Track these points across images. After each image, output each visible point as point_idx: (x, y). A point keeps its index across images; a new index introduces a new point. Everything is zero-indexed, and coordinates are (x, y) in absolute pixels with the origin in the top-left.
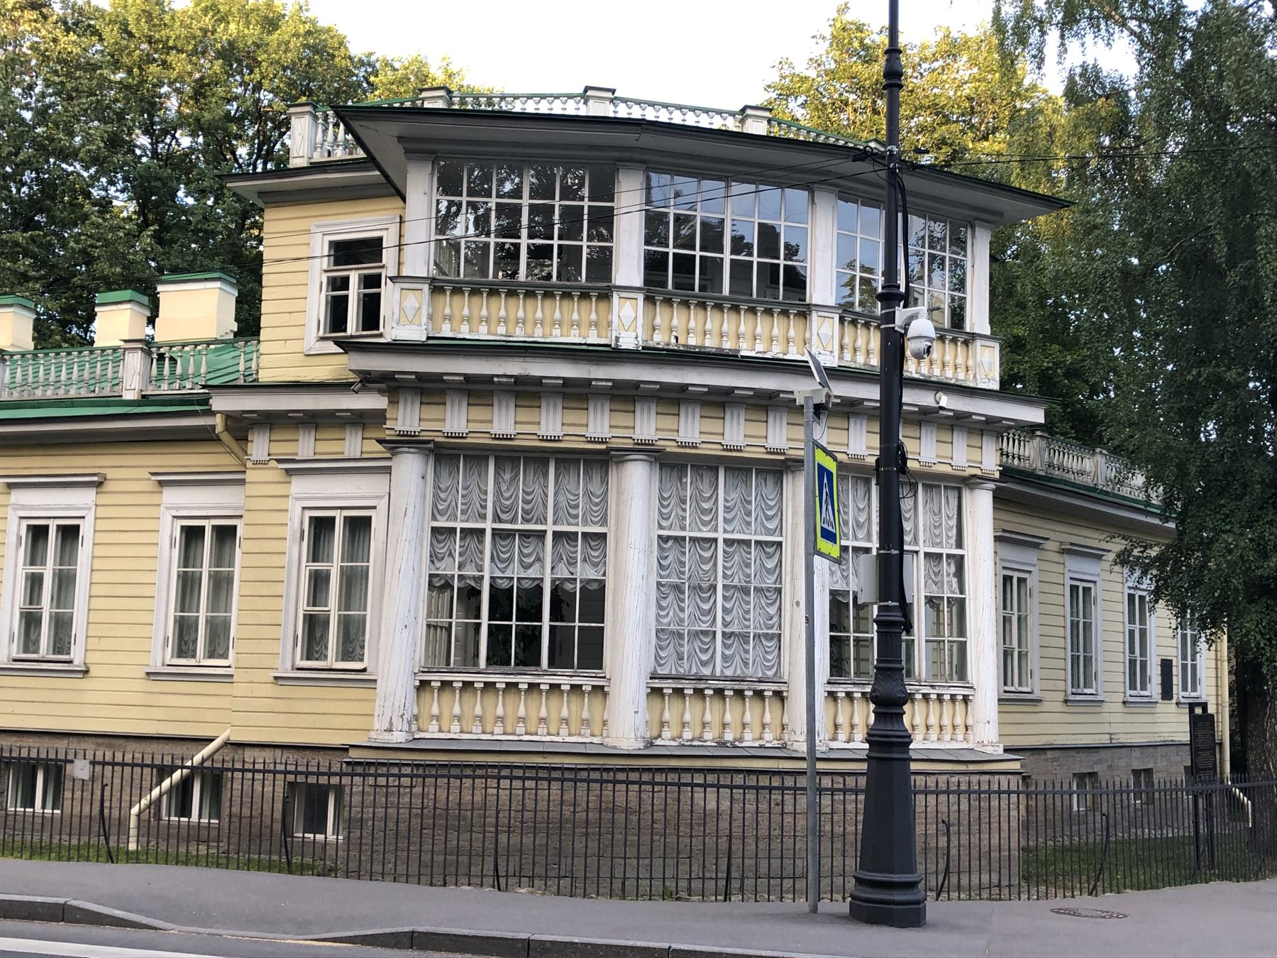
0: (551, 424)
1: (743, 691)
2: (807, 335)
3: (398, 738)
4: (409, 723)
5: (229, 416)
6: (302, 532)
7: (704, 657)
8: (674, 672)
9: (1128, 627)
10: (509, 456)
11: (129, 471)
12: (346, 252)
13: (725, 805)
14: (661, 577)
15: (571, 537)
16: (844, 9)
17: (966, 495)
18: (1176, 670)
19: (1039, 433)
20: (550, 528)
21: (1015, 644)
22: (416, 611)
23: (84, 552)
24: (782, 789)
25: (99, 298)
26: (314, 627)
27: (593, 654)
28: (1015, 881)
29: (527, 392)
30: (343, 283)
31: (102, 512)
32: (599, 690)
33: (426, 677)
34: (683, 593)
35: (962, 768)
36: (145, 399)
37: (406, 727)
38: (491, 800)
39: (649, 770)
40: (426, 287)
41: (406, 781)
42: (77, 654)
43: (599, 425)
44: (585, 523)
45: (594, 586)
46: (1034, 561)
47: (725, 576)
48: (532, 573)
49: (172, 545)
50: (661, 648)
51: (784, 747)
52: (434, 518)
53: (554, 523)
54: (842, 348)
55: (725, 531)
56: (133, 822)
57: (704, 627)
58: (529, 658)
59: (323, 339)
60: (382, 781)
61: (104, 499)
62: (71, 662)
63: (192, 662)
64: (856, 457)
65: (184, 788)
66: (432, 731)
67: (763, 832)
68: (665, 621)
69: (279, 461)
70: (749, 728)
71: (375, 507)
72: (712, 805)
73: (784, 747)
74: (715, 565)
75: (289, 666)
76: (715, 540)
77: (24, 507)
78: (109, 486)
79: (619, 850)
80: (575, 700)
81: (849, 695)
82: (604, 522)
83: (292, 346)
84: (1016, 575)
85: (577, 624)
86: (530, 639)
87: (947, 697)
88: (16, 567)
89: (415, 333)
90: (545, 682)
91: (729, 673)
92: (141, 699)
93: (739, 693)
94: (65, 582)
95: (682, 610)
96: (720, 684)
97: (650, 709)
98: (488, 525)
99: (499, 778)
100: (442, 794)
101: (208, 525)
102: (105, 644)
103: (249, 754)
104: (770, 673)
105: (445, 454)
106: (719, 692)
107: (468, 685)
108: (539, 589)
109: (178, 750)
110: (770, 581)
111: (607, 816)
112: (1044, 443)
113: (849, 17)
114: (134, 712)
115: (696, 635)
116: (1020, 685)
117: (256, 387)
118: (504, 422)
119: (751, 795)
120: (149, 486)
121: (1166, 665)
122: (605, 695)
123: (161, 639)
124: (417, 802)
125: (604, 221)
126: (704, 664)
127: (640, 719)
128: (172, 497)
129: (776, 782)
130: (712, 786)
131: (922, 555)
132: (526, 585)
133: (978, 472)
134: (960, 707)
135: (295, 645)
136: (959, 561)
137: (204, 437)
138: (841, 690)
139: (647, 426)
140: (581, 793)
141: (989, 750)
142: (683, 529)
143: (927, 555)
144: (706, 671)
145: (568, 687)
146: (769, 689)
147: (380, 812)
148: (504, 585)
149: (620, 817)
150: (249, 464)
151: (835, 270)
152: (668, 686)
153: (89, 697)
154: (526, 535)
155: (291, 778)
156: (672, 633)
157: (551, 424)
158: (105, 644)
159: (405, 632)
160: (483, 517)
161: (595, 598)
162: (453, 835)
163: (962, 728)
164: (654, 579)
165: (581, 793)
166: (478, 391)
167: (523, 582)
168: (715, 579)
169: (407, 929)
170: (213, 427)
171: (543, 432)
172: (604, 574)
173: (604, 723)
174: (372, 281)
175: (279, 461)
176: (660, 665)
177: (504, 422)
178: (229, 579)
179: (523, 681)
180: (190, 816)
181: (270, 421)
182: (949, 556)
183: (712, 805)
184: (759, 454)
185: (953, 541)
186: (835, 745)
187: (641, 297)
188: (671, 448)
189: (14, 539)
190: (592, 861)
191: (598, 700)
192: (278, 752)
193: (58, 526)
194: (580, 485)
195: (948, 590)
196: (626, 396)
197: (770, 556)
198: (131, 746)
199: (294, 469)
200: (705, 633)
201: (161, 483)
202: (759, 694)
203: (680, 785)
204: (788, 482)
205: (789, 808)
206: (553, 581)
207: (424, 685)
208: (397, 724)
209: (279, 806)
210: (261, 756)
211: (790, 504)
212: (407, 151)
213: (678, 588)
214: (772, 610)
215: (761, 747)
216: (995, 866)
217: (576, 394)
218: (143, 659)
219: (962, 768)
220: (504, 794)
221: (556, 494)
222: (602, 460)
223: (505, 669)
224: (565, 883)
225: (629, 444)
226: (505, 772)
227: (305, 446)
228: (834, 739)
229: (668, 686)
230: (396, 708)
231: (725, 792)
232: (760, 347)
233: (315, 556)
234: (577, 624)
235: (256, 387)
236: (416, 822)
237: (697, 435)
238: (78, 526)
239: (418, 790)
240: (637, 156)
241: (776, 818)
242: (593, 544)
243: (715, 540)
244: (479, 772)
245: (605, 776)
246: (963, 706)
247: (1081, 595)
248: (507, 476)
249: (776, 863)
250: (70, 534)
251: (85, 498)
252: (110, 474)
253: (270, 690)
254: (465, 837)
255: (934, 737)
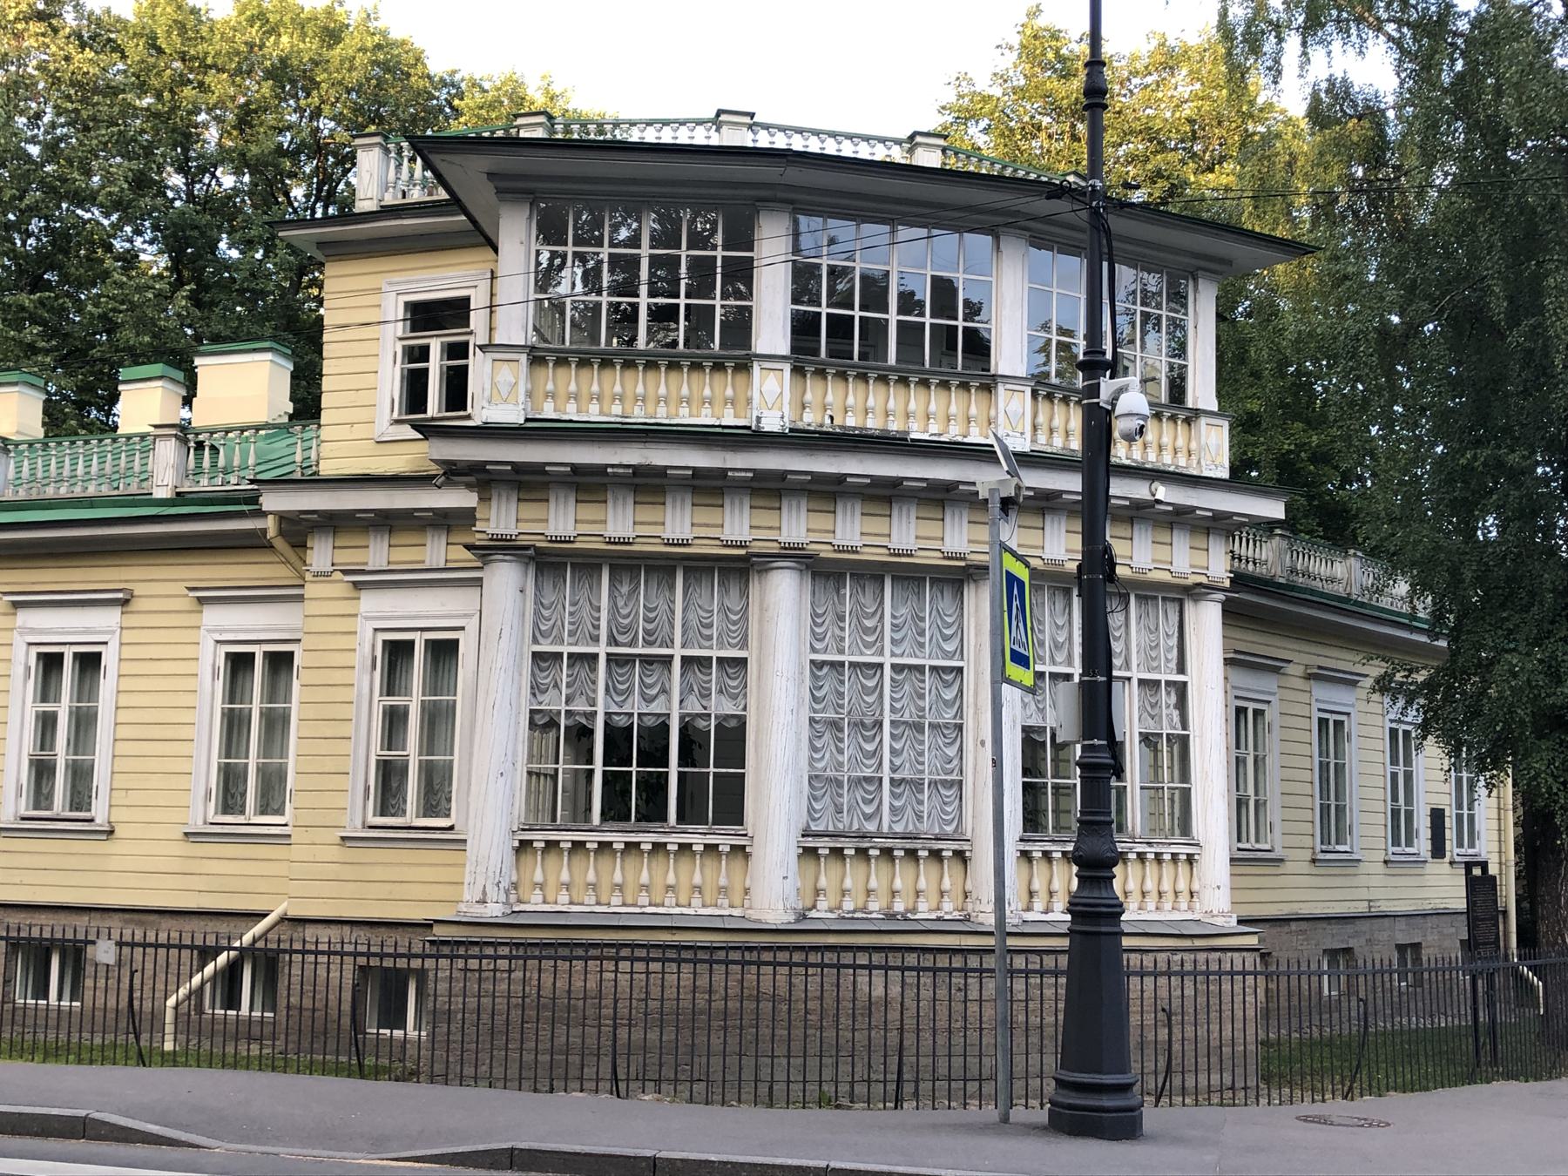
0: (678, 524)
1: (916, 851)
2: (993, 413)
3: (493, 911)
4: (507, 892)
5: (283, 518)
6: (367, 789)
7: (869, 810)
8: (831, 828)
9: (1389, 768)
10: (628, 565)
11: (161, 586)
12: (425, 315)
13: (895, 990)
14: (815, 711)
15: (704, 662)
16: (1035, 12)
17: (1189, 607)
18: (1450, 823)
19: (1278, 531)
20: (678, 652)
21: (1251, 791)
22: (515, 754)
23: (107, 685)
24: (965, 971)
25: (124, 373)
26: (390, 775)
27: (731, 807)
28: (1252, 1083)
29: (649, 485)
30: (422, 354)
31: (129, 636)
32: (740, 851)
33: (810, 843)
34: (841, 730)
35: (1187, 943)
36: (180, 498)
37: (503, 898)
38: (608, 987)
39: (802, 948)
40: (523, 358)
41: (503, 964)
42: (99, 811)
43: (738, 526)
44: (721, 646)
45: (733, 723)
46: (1274, 688)
47: (893, 710)
48: (656, 707)
49: (215, 676)
50: (815, 799)
51: (967, 919)
52: (535, 641)
53: (672, 656)
54: (1035, 428)
55: (893, 654)
56: (169, 1016)
57: (868, 773)
58: (653, 811)
59: (398, 422)
60: (473, 964)
61: (132, 620)
62: (92, 820)
63: (240, 819)
64: (1053, 562)
65: (231, 975)
66: (535, 902)
67: (942, 1023)
68: (820, 765)
69: (345, 572)
70: (923, 896)
71: (463, 628)
72: (878, 991)
73: (967, 919)
74: (881, 696)
75: (359, 824)
76: (881, 666)
77: (33, 631)
78: (136, 605)
79: (765, 1047)
80: (710, 863)
81: (1047, 855)
82: (744, 644)
83: (360, 432)
84: (1251, 706)
85: (712, 769)
86: (654, 789)
87: (1167, 857)
88: (23, 704)
89: (512, 415)
90: (673, 841)
91: (898, 828)
92: (176, 865)
93: (912, 854)
94: (84, 722)
95: (841, 751)
96: (889, 843)
97: (801, 873)
98: (602, 650)
99: (617, 960)
100: (547, 979)
101: (258, 651)
102: (134, 797)
103: (310, 933)
104: (949, 829)
105: (548, 562)
106: (887, 853)
107: (578, 846)
108: (664, 728)
109: (223, 927)
110: (948, 716)
111: (750, 1005)
112: (1284, 544)
113: (1041, 22)
114: (171, 882)
115: (858, 782)
116: (1257, 841)
117: (316, 482)
118: (620, 522)
119: (973, 981)
120: (185, 604)
121: (1437, 816)
122: (747, 856)
123: (202, 793)
124: (517, 988)
125: (741, 274)
126: (868, 817)
127: (790, 886)
128: (215, 617)
129: (957, 962)
130: (862, 967)
131: (1135, 682)
132: (650, 722)
133: (1204, 580)
134: (1183, 868)
135: (367, 797)
136: (1181, 690)
137: (253, 543)
138: (1036, 849)
139: (796, 526)
140: (719, 977)
141: (1219, 921)
142: (841, 652)
143: (1141, 682)
144: (871, 827)
145: (728, 849)
146: (947, 848)
147: (472, 1002)
148: (622, 722)
149: (766, 1006)
150: (308, 577)
151: (1026, 333)
152: (824, 845)
153: (114, 863)
154: (648, 661)
155: (362, 961)
156: (829, 780)
157: (678, 524)
158: (134, 797)
159: (501, 780)
160: (596, 639)
161: (733, 738)
162: (561, 1030)
163: (1186, 894)
164: (806, 714)
165: (719, 977)
166: (588, 484)
167: (645, 719)
168: (881, 714)
169: (648, 1153)
170: (264, 531)
171: (668, 534)
172: (745, 709)
173: (746, 891)
174: (457, 351)
175: (345, 572)
176: (814, 820)
177: (620, 522)
178: (285, 718)
179: (646, 840)
180: (239, 1009)
181: (334, 523)
182: (1168, 683)
183: (878, 991)
184: (934, 559)
185: (1173, 665)
186: (1029, 916)
187: (787, 367)
188: (826, 552)
189: (20, 670)
190: (732, 1061)
191: (738, 863)
192: (347, 929)
193: (75, 654)
194: (714, 599)
195: (1168, 725)
196: (770, 490)
197: (948, 685)
198: (167, 923)
199: (363, 582)
200: (868, 780)
201: (201, 600)
202: (936, 855)
203: (839, 967)
204: (969, 593)
205: (973, 994)
206: (682, 718)
207: (525, 845)
208: (492, 894)
209: (347, 996)
210: (325, 934)
211: (972, 620)
212: (499, 191)
213: (835, 725)
214: (952, 752)
215: (939, 919)
216: (1227, 1064)
217: (708, 488)
218: (176, 816)
219: (1187, 943)
220: (624, 980)
221: (684, 610)
222: (740, 568)
223: (702, 828)
224: (699, 1088)
225: (773, 548)
226: (625, 952)
227: (377, 553)
228: (1029, 909)
229: (824, 845)
230: (490, 874)
231: (895, 976)
232: (934, 428)
233: (390, 688)
234: (712, 769)
235: (316, 482)
236: (515, 1014)
237: (858, 537)
238: (100, 654)
239: (518, 975)
240: (780, 195)
241: (958, 1007)
242: (730, 671)
243: (881, 666)
244: (592, 952)
245: (747, 956)
246: (1187, 867)
247: (1331, 730)
248: (625, 589)
249: (957, 1062)
250: (89, 663)
251: (112, 617)
252: (139, 589)
253: (336, 853)
254: (576, 1032)
255: (1151, 905)
